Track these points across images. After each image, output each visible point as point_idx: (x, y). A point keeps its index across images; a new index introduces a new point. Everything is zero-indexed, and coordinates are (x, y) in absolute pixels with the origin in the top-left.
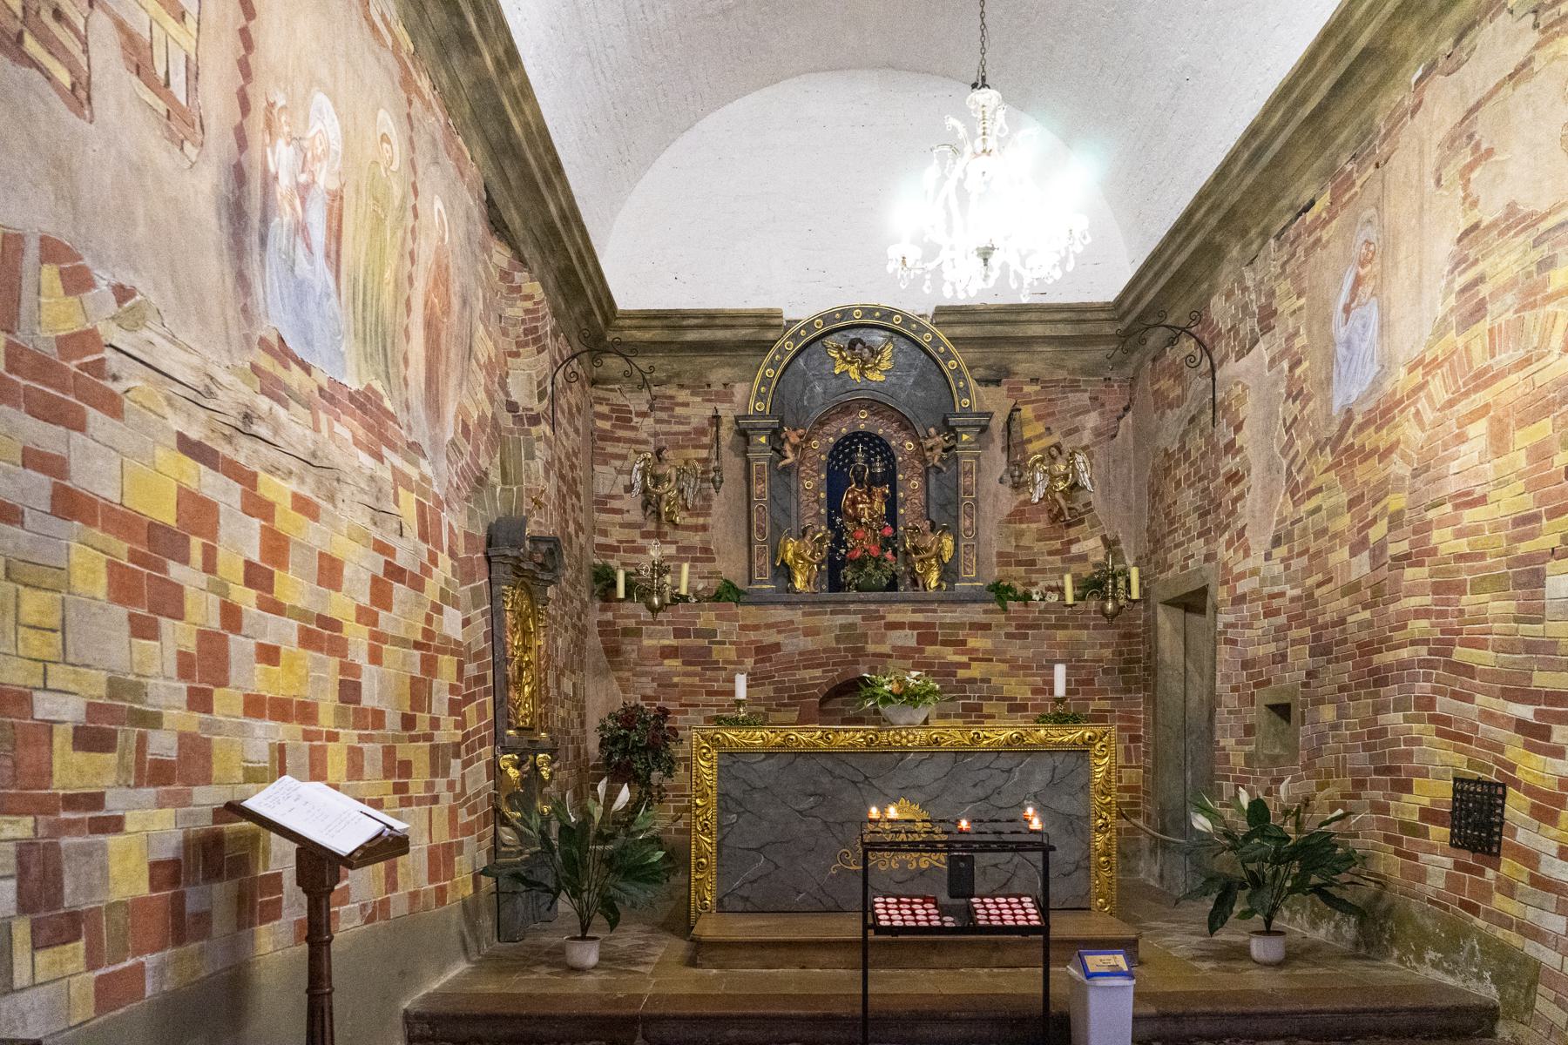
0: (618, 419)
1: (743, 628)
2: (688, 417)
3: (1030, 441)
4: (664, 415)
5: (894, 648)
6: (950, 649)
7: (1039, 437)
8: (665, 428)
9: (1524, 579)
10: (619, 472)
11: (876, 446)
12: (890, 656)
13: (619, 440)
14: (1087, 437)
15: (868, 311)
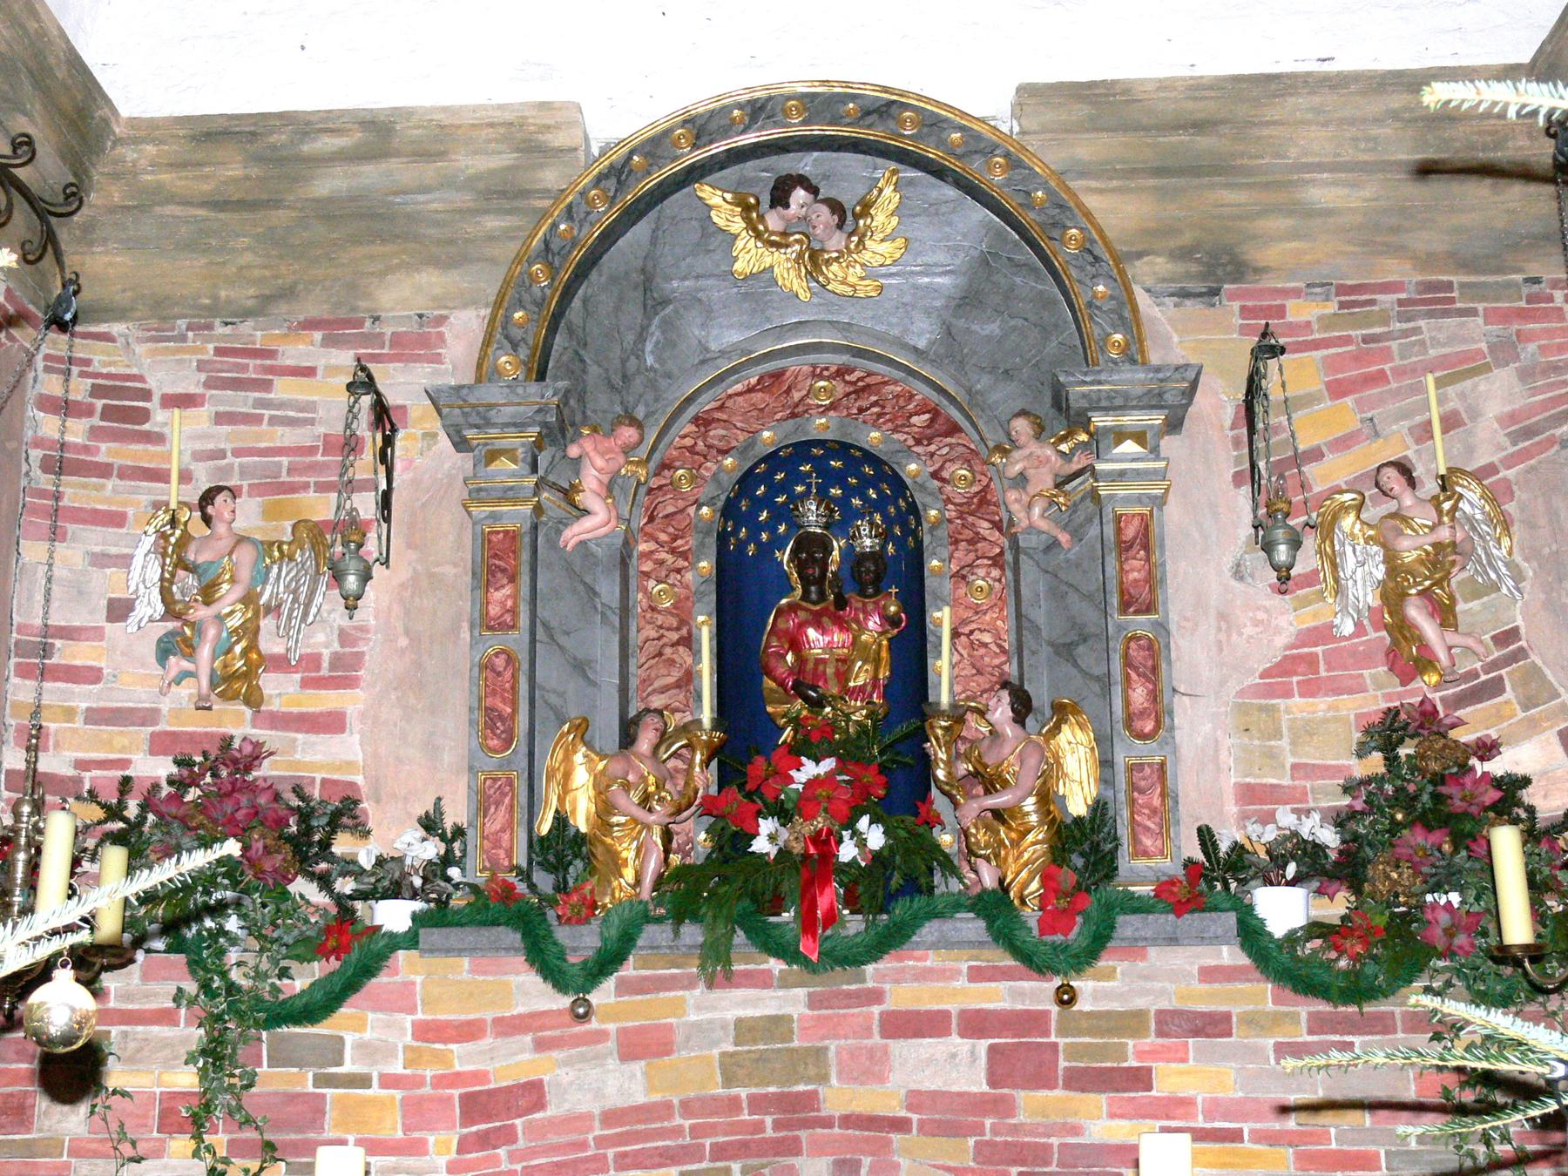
0: (107, 413)
1: (424, 1031)
2: (311, 407)
3: (1316, 455)
4: (242, 402)
5: (916, 1100)
6: (1101, 1101)
7: (1343, 443)
8: (245, 435)
9: (1181, 1111)
10: (101, 560)
11: (866, 482)
12: (900, 1125)
13: (104, 471)
14: (1487, 443)
15: (819, 104)
